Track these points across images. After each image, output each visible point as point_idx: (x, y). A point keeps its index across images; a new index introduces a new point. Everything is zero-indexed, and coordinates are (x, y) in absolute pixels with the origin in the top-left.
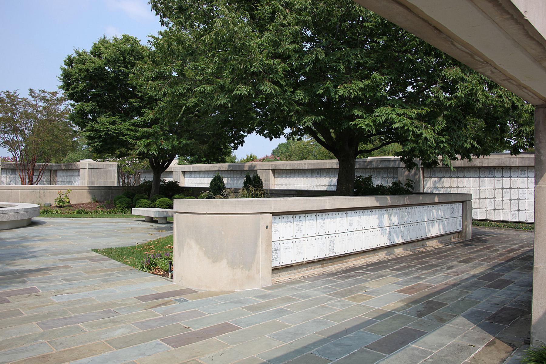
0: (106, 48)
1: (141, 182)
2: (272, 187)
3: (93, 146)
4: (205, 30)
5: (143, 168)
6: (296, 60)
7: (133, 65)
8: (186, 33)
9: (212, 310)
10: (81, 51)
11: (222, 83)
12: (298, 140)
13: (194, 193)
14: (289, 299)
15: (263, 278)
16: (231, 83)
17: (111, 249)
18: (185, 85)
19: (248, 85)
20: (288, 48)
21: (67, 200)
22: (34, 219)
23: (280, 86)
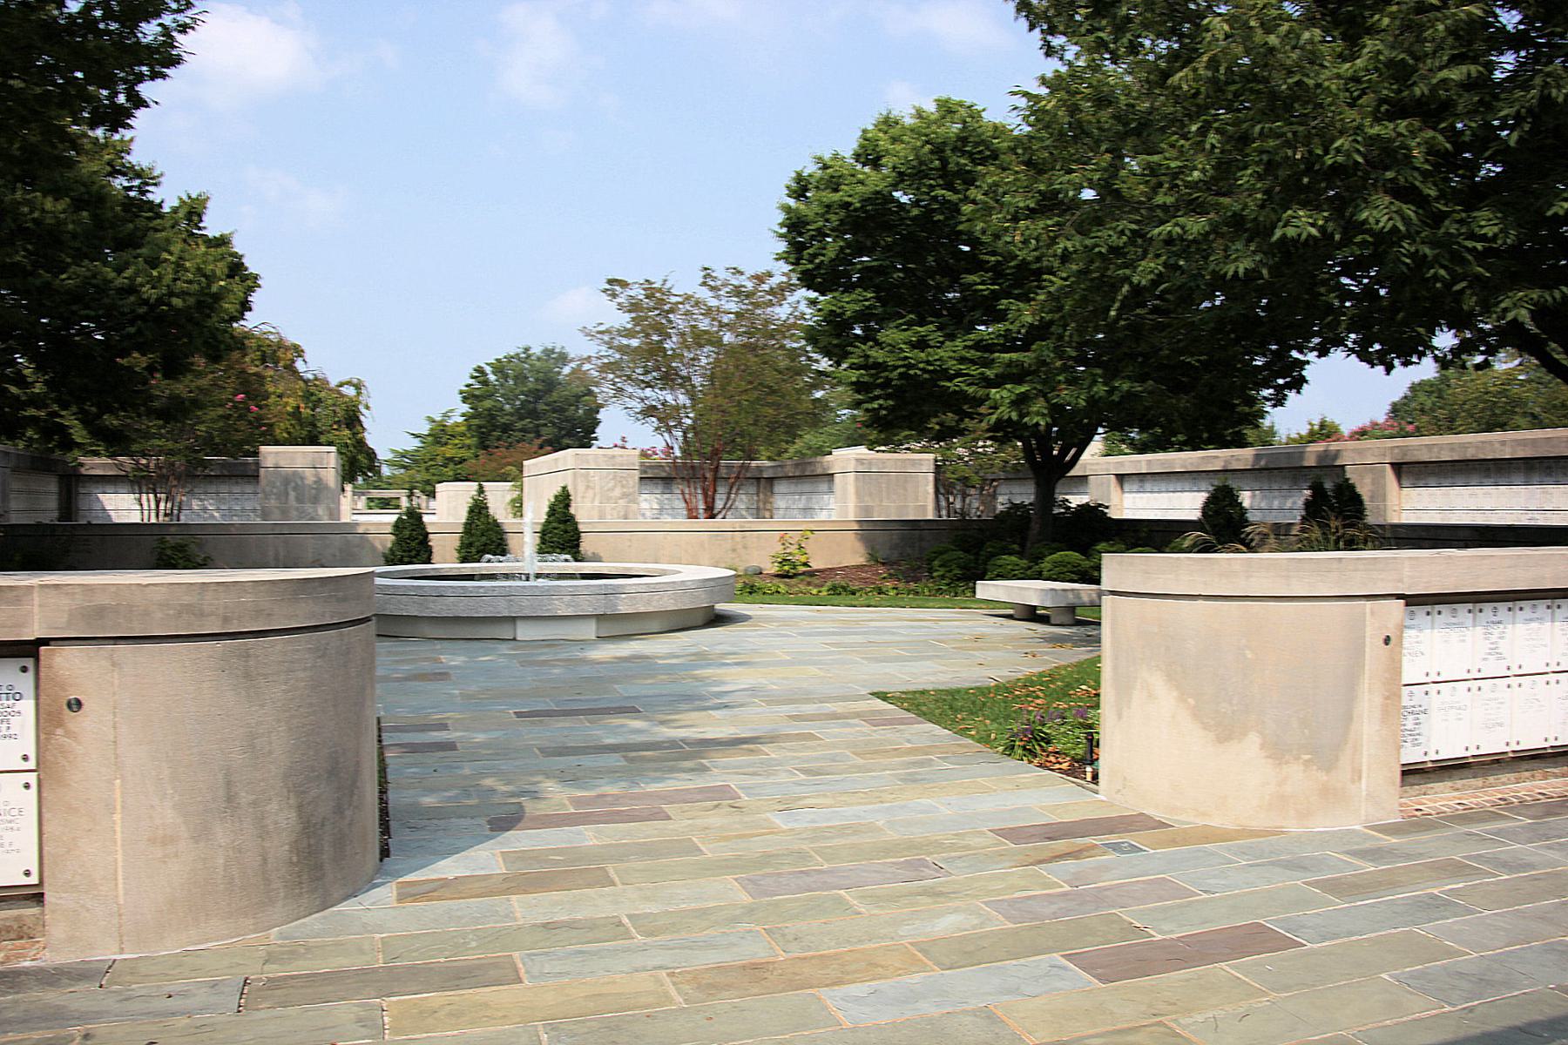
0: (894, 140)
1: (1000, 508)
2: (1394, 519)
3: (867, 410)
4: (1173, 56)
5: (1003, 469)
6: (1471, 114)
7: (970, 180)
8: (1117, 73)
9: (1212, 881)
10: (827, 156)
11: (1237, 207)
12: (1478, 367)
13: (1155, 536)
14: (1457, 870)
15: (1373, 799)
16: (1262, 207)
17: (923, 692)
18: (1122, 224)
19: (1319, 208)
20: (1444, 81)
21: (803, 559)
22: (721, 607)
23: (1419, 200)
